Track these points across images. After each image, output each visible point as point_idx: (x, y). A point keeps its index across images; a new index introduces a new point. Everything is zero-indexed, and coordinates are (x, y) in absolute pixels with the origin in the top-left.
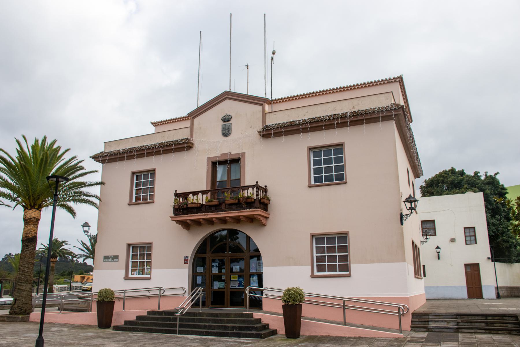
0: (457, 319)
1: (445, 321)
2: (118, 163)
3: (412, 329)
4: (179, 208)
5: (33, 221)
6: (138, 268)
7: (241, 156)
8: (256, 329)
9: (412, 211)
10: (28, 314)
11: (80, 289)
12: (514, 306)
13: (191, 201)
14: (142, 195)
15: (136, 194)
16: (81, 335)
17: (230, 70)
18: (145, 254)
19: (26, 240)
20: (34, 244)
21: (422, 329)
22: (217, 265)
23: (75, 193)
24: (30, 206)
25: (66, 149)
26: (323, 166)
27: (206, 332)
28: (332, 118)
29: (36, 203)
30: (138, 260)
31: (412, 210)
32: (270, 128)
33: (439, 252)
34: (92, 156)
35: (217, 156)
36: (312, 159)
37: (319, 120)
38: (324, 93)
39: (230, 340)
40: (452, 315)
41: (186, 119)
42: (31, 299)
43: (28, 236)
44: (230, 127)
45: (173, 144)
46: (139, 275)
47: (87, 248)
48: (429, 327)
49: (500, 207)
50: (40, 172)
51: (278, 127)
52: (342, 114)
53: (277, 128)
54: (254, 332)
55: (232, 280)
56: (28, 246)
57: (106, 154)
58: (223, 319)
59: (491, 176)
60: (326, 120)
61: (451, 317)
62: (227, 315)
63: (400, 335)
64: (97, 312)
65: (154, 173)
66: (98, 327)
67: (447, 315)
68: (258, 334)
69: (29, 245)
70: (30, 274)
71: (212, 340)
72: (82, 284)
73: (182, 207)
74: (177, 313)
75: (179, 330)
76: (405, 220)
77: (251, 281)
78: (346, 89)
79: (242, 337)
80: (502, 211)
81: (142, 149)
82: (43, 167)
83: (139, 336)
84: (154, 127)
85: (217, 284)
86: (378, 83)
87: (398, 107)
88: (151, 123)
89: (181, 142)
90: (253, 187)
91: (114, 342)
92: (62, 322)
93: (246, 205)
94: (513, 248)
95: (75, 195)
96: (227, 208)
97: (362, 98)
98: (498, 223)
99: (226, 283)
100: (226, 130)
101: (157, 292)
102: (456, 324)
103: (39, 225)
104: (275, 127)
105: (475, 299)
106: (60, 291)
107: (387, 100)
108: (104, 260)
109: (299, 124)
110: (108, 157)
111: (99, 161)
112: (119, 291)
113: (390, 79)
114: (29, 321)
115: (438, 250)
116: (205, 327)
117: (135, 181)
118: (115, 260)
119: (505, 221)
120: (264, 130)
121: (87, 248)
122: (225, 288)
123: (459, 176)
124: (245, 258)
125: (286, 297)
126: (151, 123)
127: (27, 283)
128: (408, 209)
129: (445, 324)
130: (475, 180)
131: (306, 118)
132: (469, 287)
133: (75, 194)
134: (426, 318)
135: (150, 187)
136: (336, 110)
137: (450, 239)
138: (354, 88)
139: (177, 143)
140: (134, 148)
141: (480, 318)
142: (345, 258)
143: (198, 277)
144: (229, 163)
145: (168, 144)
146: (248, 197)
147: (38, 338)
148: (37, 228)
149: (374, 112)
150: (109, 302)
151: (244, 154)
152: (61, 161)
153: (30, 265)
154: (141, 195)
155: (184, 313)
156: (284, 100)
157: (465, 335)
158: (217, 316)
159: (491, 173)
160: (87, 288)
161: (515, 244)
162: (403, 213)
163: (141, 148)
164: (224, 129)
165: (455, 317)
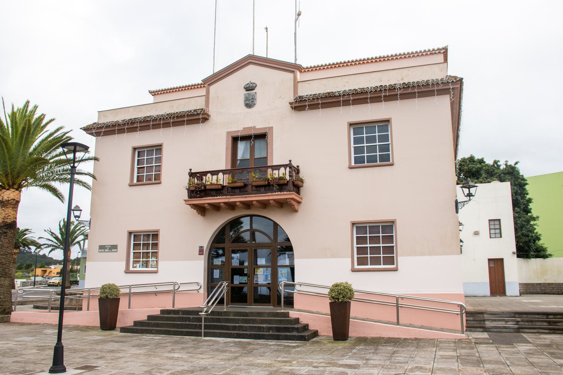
0: (515, 318)
1: (504, 320)
2: (116, 136)
3: (467, 329)
4: (196, 189)
5: (12, 203)
6: (141, 260)
7: (268, 130)
8: (297, 330)
9: (470, 198)
10: (7, 313)
11: (46, 284)
12: (556, 303)
13: (210, 181)
14: (146, 175)
15: (138, 173)
16: (86, 339)
17: (254, 30)
18: (150, 243)
19: (4, 226)
20: (13, 231)
21: (479, 329)
22: (238, 257)
23: (63, 171)
24: (8, 185)
25: (51, 119)
26: (365, 145)
27: (237, 334)
28: (379, 90)
29: (15, 182)
30: (141, 251)
31: (470, 196)
32: (304, 99)
33: (461, 246)
34: (84, 127)
35: (239, 131)
36: (352, 136)
37: (363, 92)
38: (361, 62)
39: (271, 343)
40: (509, 313)
41: (191, 88)
42: (10, 296)
43: (5, 221)
44: (254, 96)
45: (158, 119)
46: (142, 267)
47: (57, 238)
48: (486, 327)
49: (519, 199)
50: (21, 144)
51: (314, 98)
52: (389, 85)
53: (313, 99)
54: (295, 333)
55: (255, 273)
56: (6, 233)
57: (101, 125)
58: (255, 319)
59: (510, 166)
60: (371, 91)
61: (508, 315)
62: (259, 314)
63: (462, 336)
64: (99, 311)
65: (161, 149)
66: (101, 329)
67: (504, 313)
68: (301, 335)
69: (7, 232)
70: (9, 266)
71: (249, 344)
72: (43, 278)
73: (199, 188)
74: (202, 312)
75: (204, 332)
76: (461, 207)
77: (279, 275)
78: (382, 60)
79: (282, 340)
80: (522, 203)
81: (146, 120)
82: (24, 138)
83: (158, 339)
84: (153, 97)
85: (238, 278)
86: (420, 54)
87: (456, 80)
88: (149, 91)
89: (195, 113)
90: (285, 166)
91: (133, 346)
92: (53, 323)
93: (278, 187)
94: (532, 242)
95: (64, 172)
96: (254, 191)
97: (412, 68)
98: (517, 216)
99: (249, 277)
100: (249, 100)
101: (171, 288)
102: (515, 323)
103: (19, 208)
104: (310, 98)
105: (498, 297)
106: (22, 287)
107: (442, 71)
108: (100, 251)
109: (339, 95)
110: (103, 128)
111: (93, 133)
112: (124, 287)
113: (434, 50)
114: (9, 322)
115: (461, 244)
116: (234, 328)
117: (136, 158)
118: (113, 250)
119: (523, 214)
120: (297, 101)
121: (57, 238)
122: (248, 283)
123: (478, 164)
124: (248, 249)
125: (335, 293)
126: (149, 91)
127: (5, 277)
128: (466, 195)
129: (503, 324)
130: (494, 169)
131: (347, 89)
132: (492, 283)
133: (63, 172)
134: (480, 317)
135: (155, 166)
136: (381, 81)
137: (474, 232)
138: (392, 59)
139: (190, 114)
140: (136, 119)
141: (540, 317)
142: (390, 250)
143: (215, 271)
144: (253, 139)
145: (180, 115)
146: (281, 179)
147: (56, 344)
148: (16, 211)
149: (428, 85)
150: (113, 299)
151: (271, 128)
152: (44, 133)
153: (8, 256)
154: (144, 175)
155: (209, 312)
156: (310, 70)
157: (531, 336)
158: (247, 316)
159: (511, 163)
160: (54, 282)
161: (534, 238)
162: (458, 200)
163: (145, 119)
164: (247, 99)
165: (513, 315)
